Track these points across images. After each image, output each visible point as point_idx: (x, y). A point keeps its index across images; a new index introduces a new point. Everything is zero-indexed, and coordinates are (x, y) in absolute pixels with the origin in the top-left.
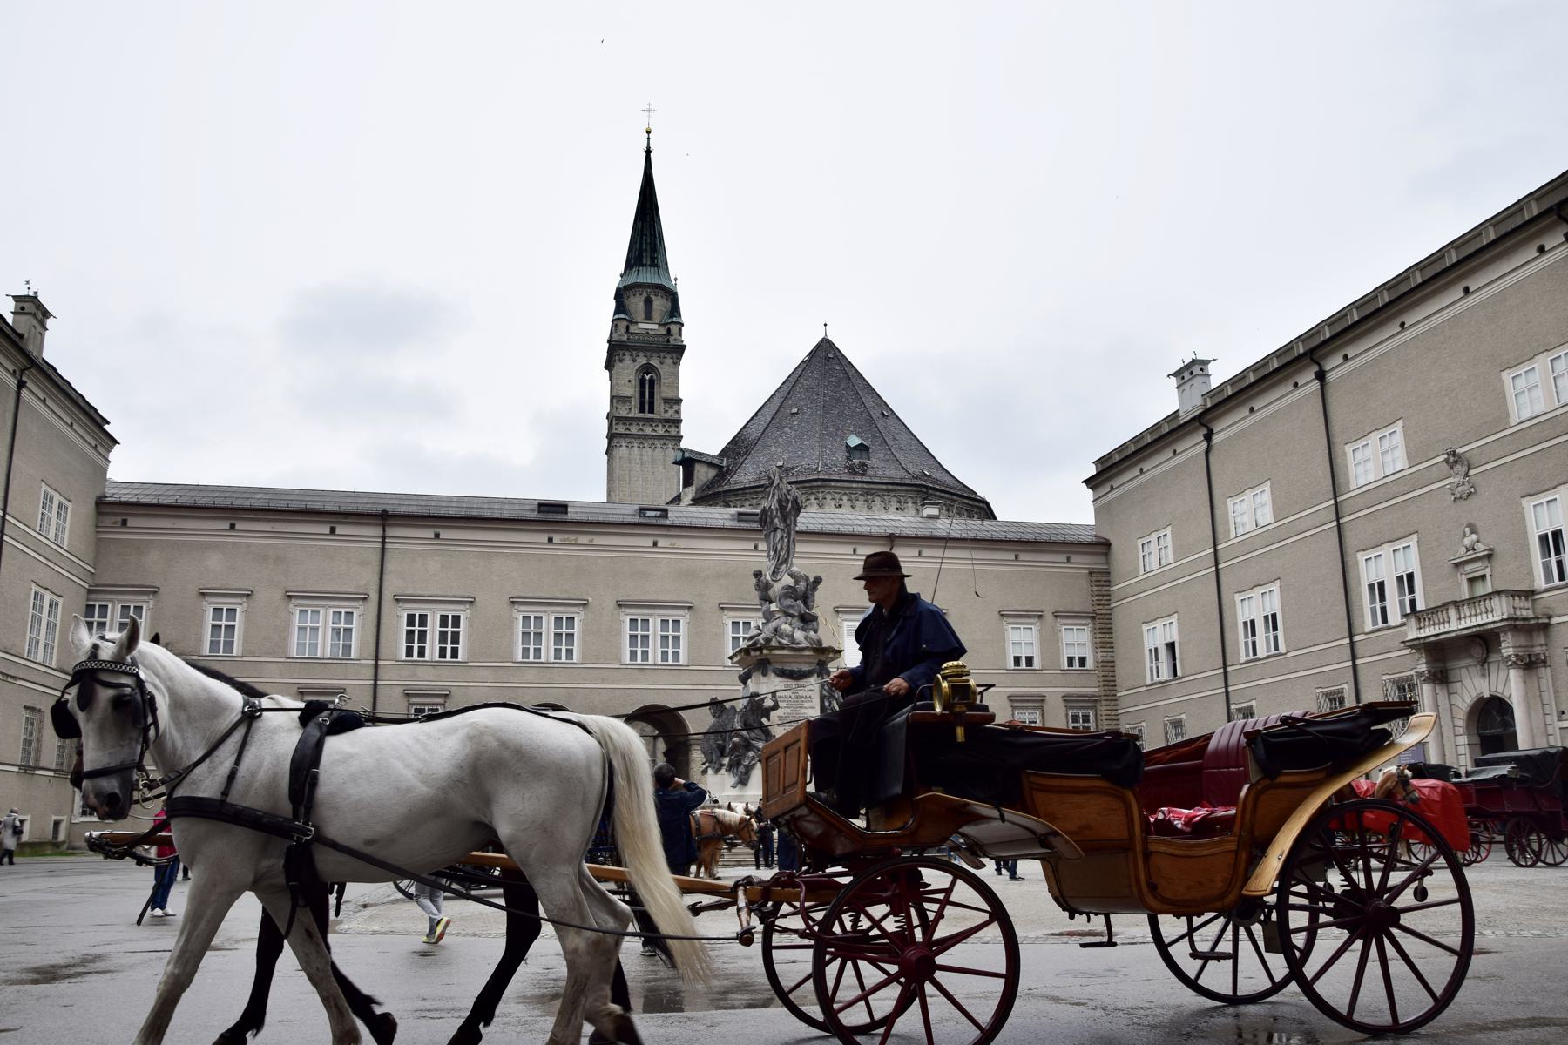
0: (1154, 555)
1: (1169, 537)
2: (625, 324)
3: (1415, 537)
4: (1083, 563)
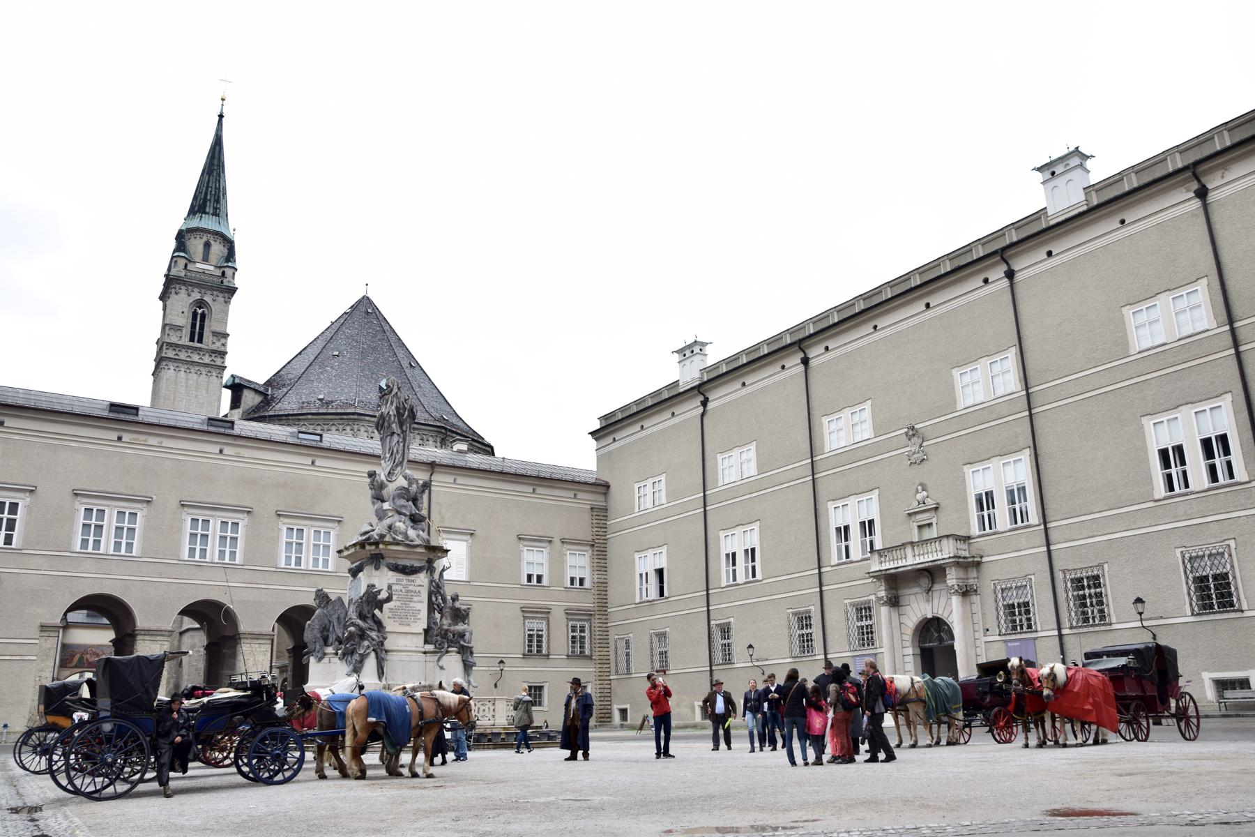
0: (647, 495)
1: (663, 482)
2: (184, 261)
3: (877, 492)
4: (588, 499)
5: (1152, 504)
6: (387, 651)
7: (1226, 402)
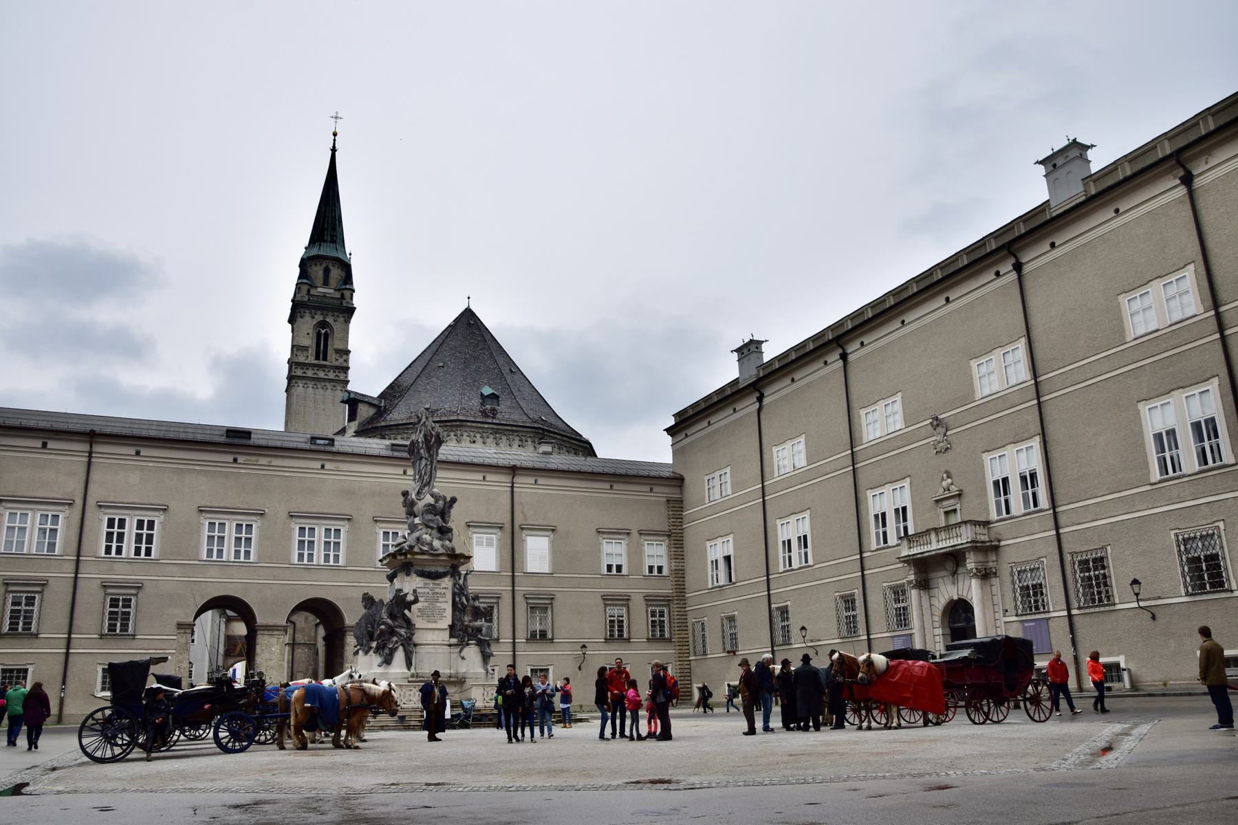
0: (718, 487)
1: (728, 475)
3: (908, 480)
4: (662, 493)
5: (1148, 488)
6: (415, 645)
7: (1213, 386)
